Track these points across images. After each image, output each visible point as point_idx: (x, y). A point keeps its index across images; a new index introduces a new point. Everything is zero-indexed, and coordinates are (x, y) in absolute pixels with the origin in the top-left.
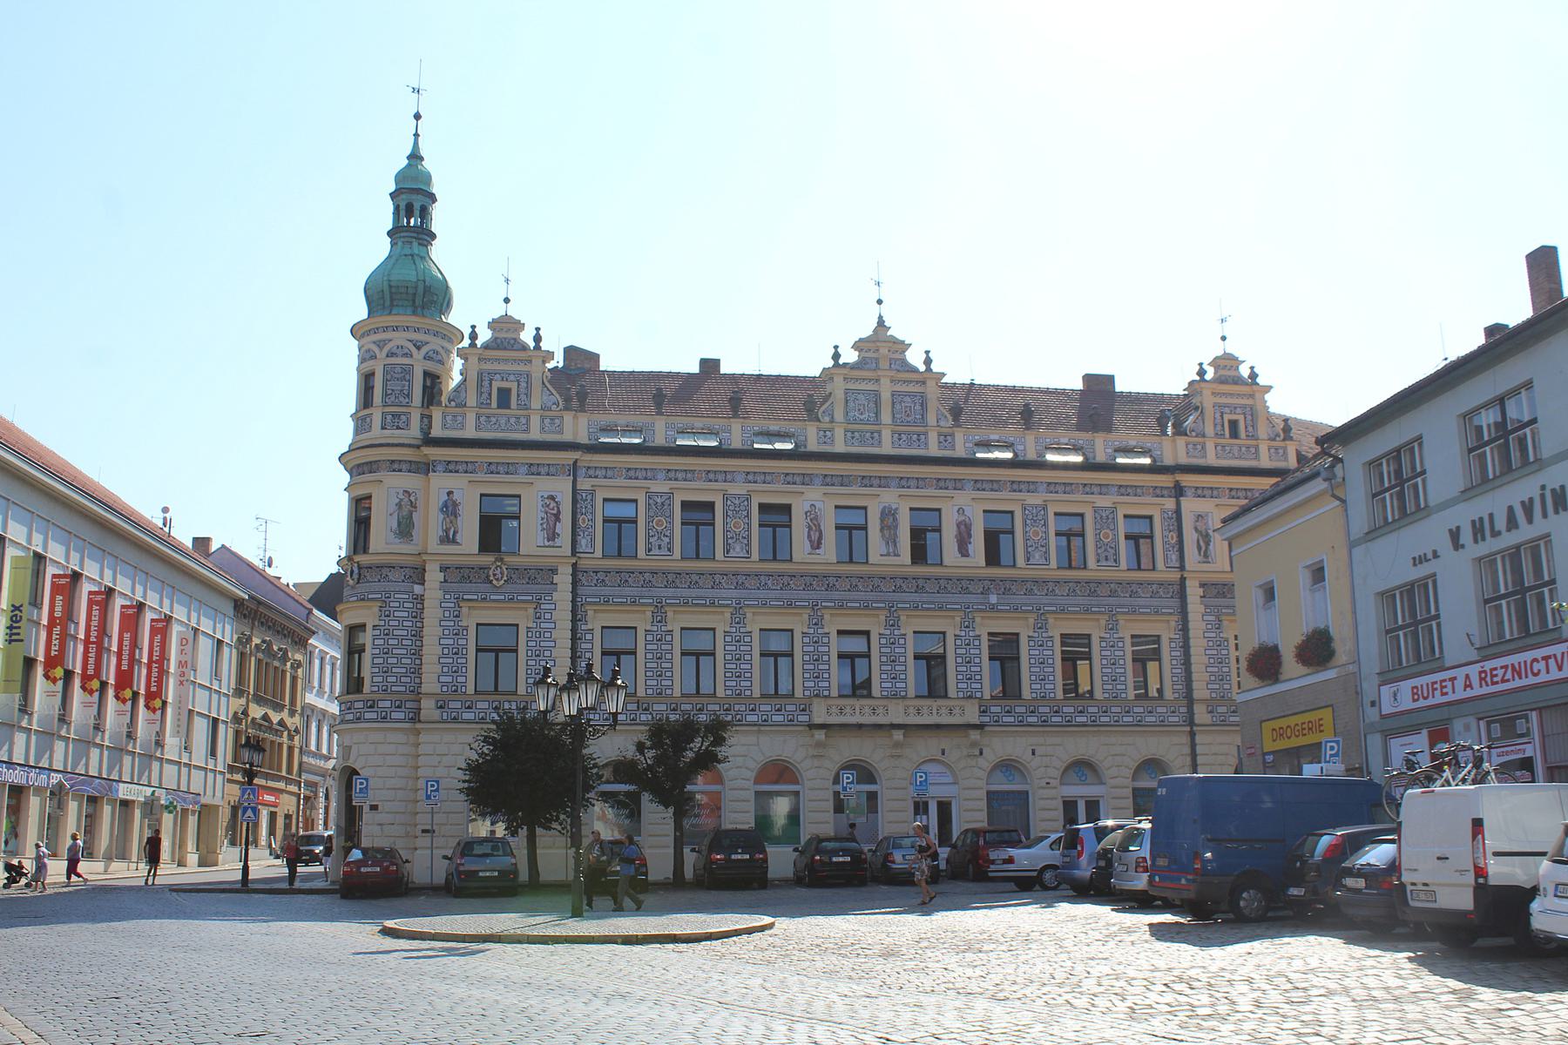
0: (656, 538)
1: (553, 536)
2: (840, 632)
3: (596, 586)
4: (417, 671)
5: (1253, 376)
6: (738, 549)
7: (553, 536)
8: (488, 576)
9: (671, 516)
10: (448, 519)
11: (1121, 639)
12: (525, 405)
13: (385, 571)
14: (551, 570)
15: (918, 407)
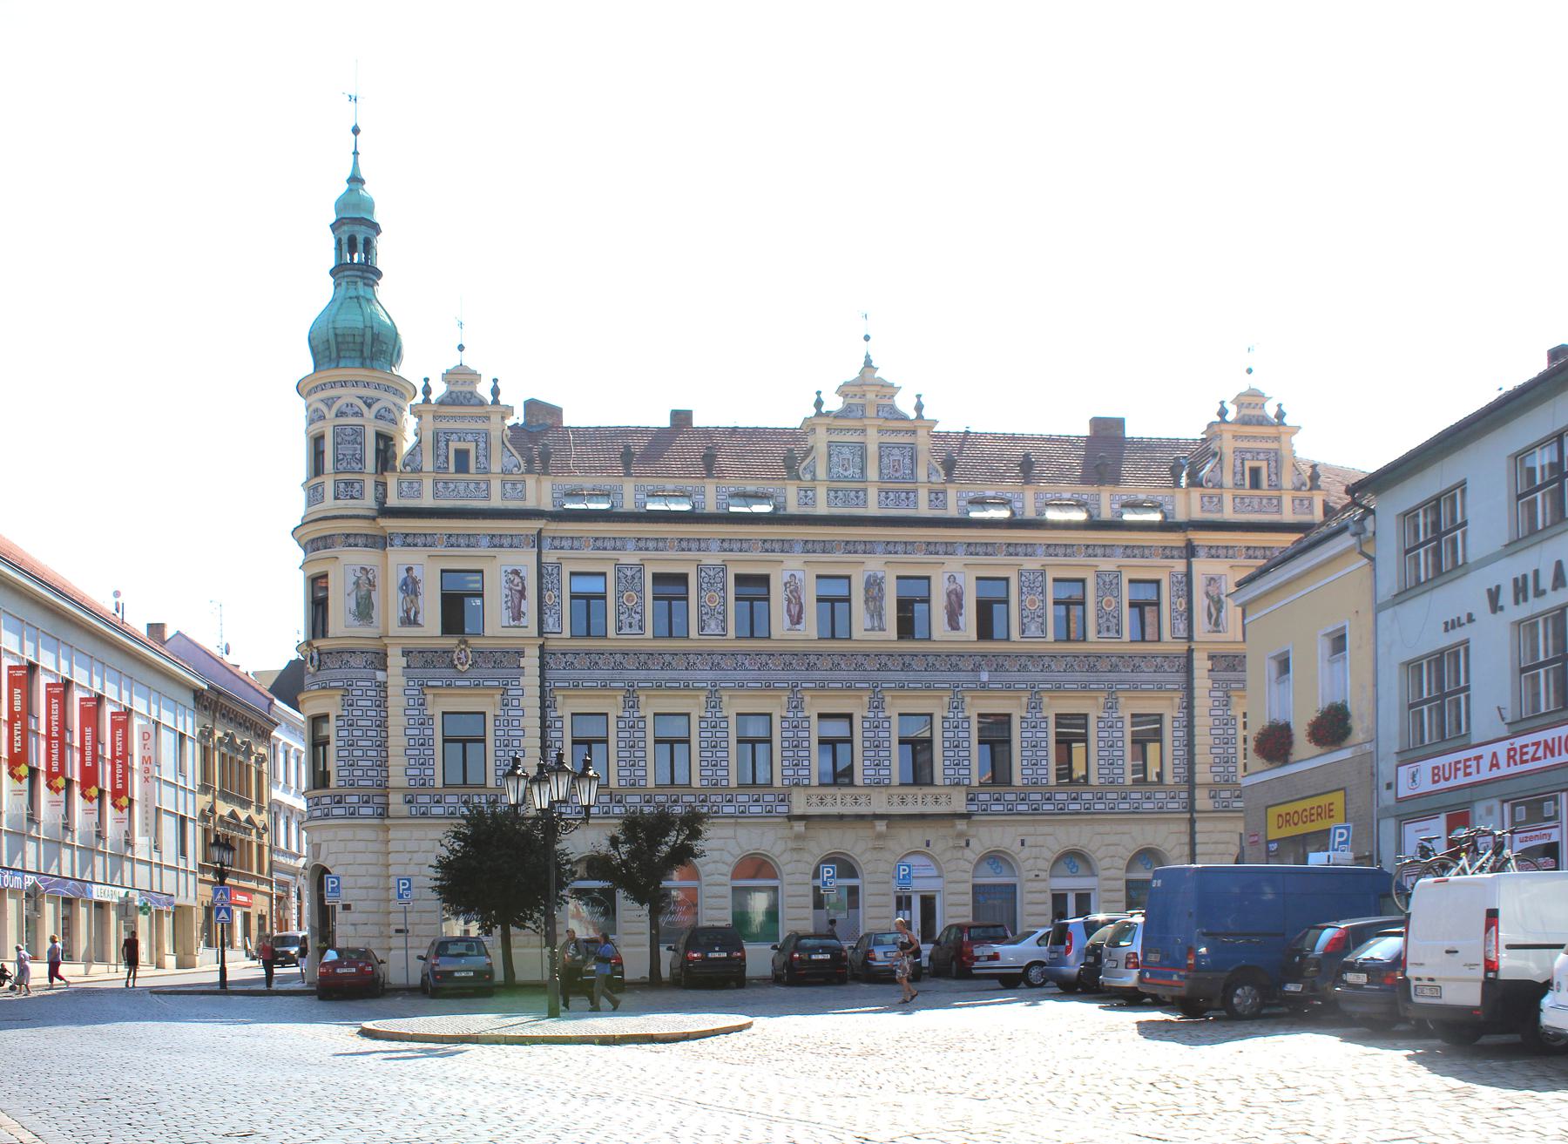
0: (626, 615)
1: (518, 615)
3: (565, 669)
4: (383, 764)
5: (1280, 415)
6: (713, 626)
7: (518, 615)
8: (452, 661)
9: (642, 591)
11: (1121, 719)
12: (485, 468)
13: (346, 657)
15: (907, 461)
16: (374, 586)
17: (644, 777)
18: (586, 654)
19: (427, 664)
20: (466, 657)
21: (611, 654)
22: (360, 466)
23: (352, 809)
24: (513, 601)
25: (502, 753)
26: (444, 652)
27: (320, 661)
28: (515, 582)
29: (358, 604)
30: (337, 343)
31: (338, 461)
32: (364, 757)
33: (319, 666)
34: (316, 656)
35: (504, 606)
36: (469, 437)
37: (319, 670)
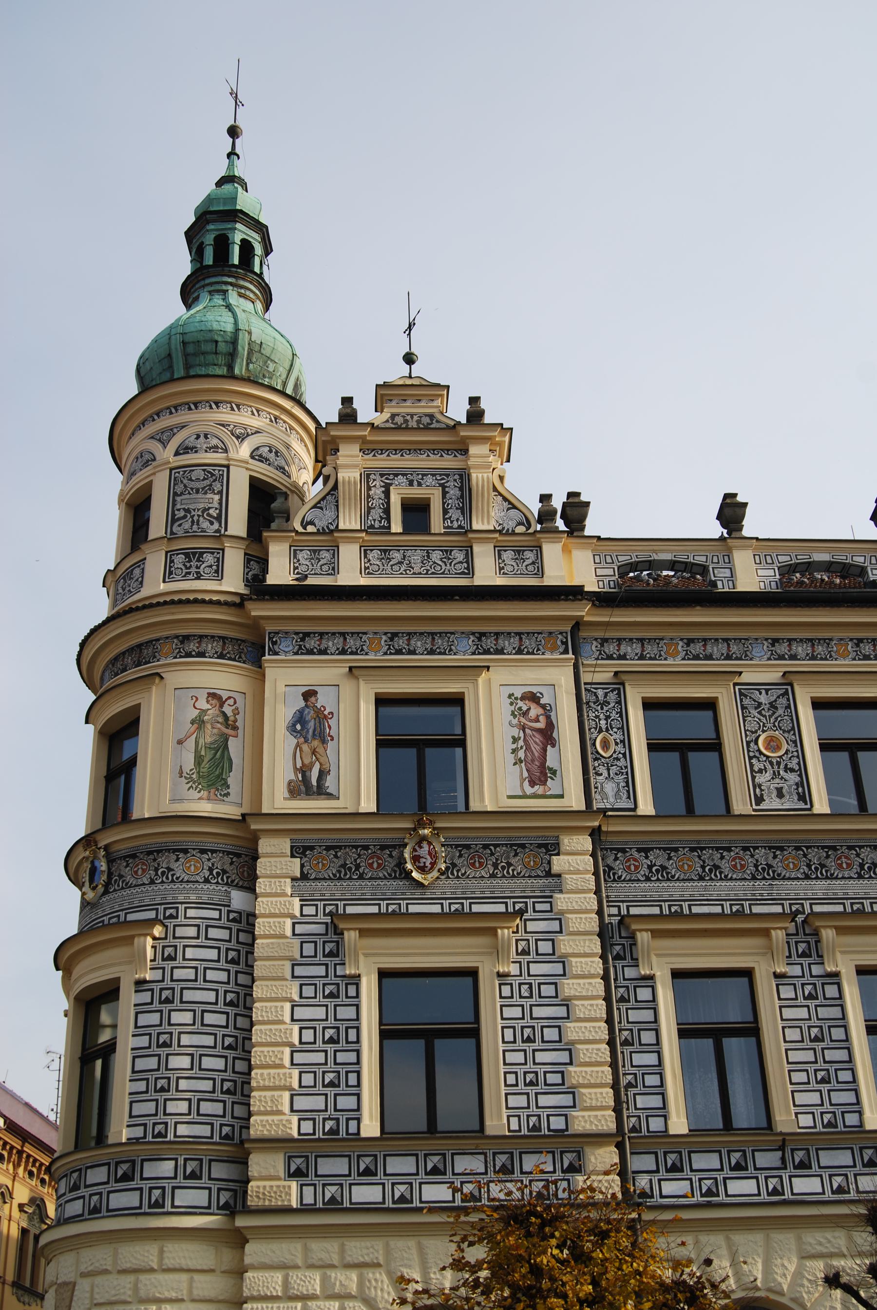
0: (768, 775)
2: (677, 974)
3: (648, 879)
5: (475, 415)
8: (401, 862)
10: (305, 747)
12: (460, 527)
13: (164, 861)
14: (545, 846)
16: (235, 728)
17: (663, 1112)
18: (692, 849)
19: (344, 873)
20: (433, 855)
21: (745, 849)
22: (216, 526)
23: (156, 1193)
24: (528, 748)
25: (519, 1057)
26: (383, 848)
27: (110, 874)
28: (533, 714)
29: (199, 760)
30: (186, 355)
31: (174, 521)
32: (198, 981)
33: (107, 885)
34: (103, 866)
35: (511, 758)
36: (429, 480)
37: (106, 892)
